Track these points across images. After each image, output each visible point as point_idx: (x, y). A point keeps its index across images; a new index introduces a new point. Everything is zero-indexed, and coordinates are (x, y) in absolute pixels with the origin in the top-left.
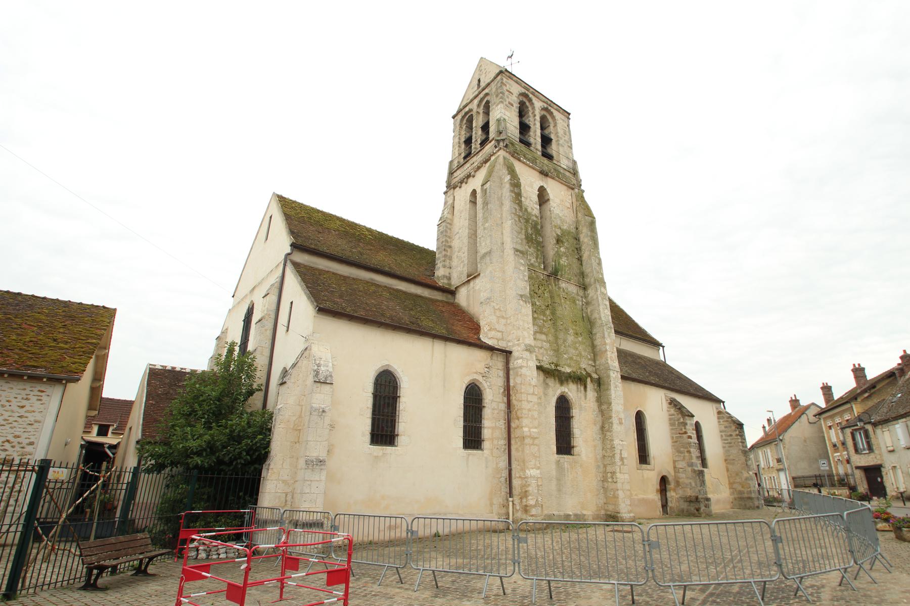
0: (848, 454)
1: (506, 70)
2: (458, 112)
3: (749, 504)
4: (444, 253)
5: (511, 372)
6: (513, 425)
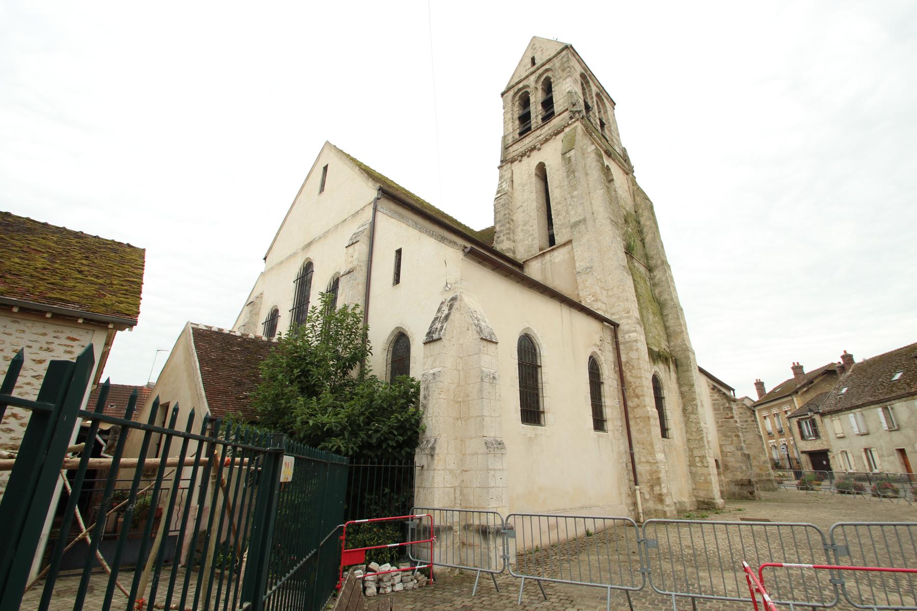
0: (794, 439)
1: (571, 46)
2: (509, 89)
3: (769, 485)
4: (508, 225)
5: (621, 347)
6: (630, 404)
